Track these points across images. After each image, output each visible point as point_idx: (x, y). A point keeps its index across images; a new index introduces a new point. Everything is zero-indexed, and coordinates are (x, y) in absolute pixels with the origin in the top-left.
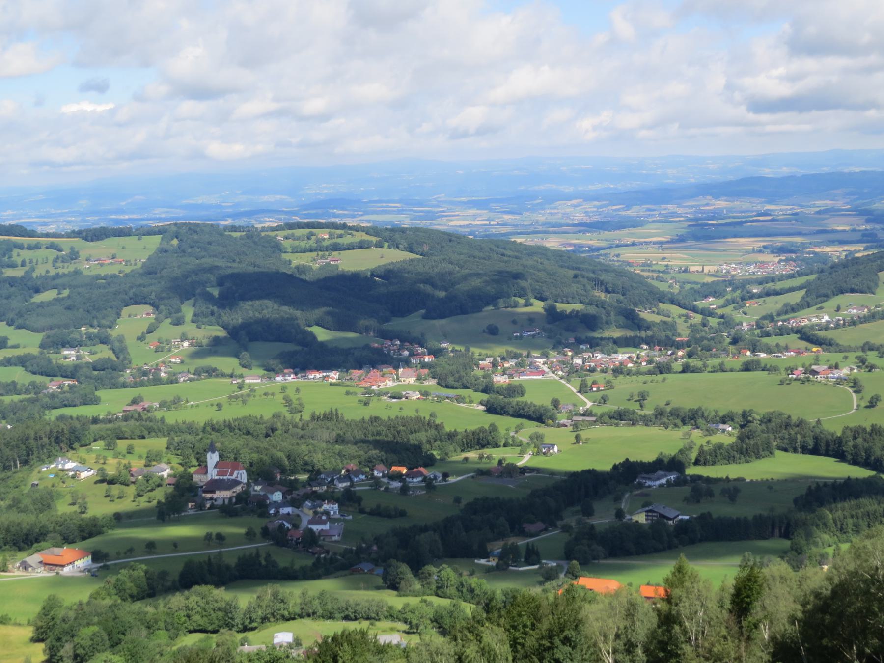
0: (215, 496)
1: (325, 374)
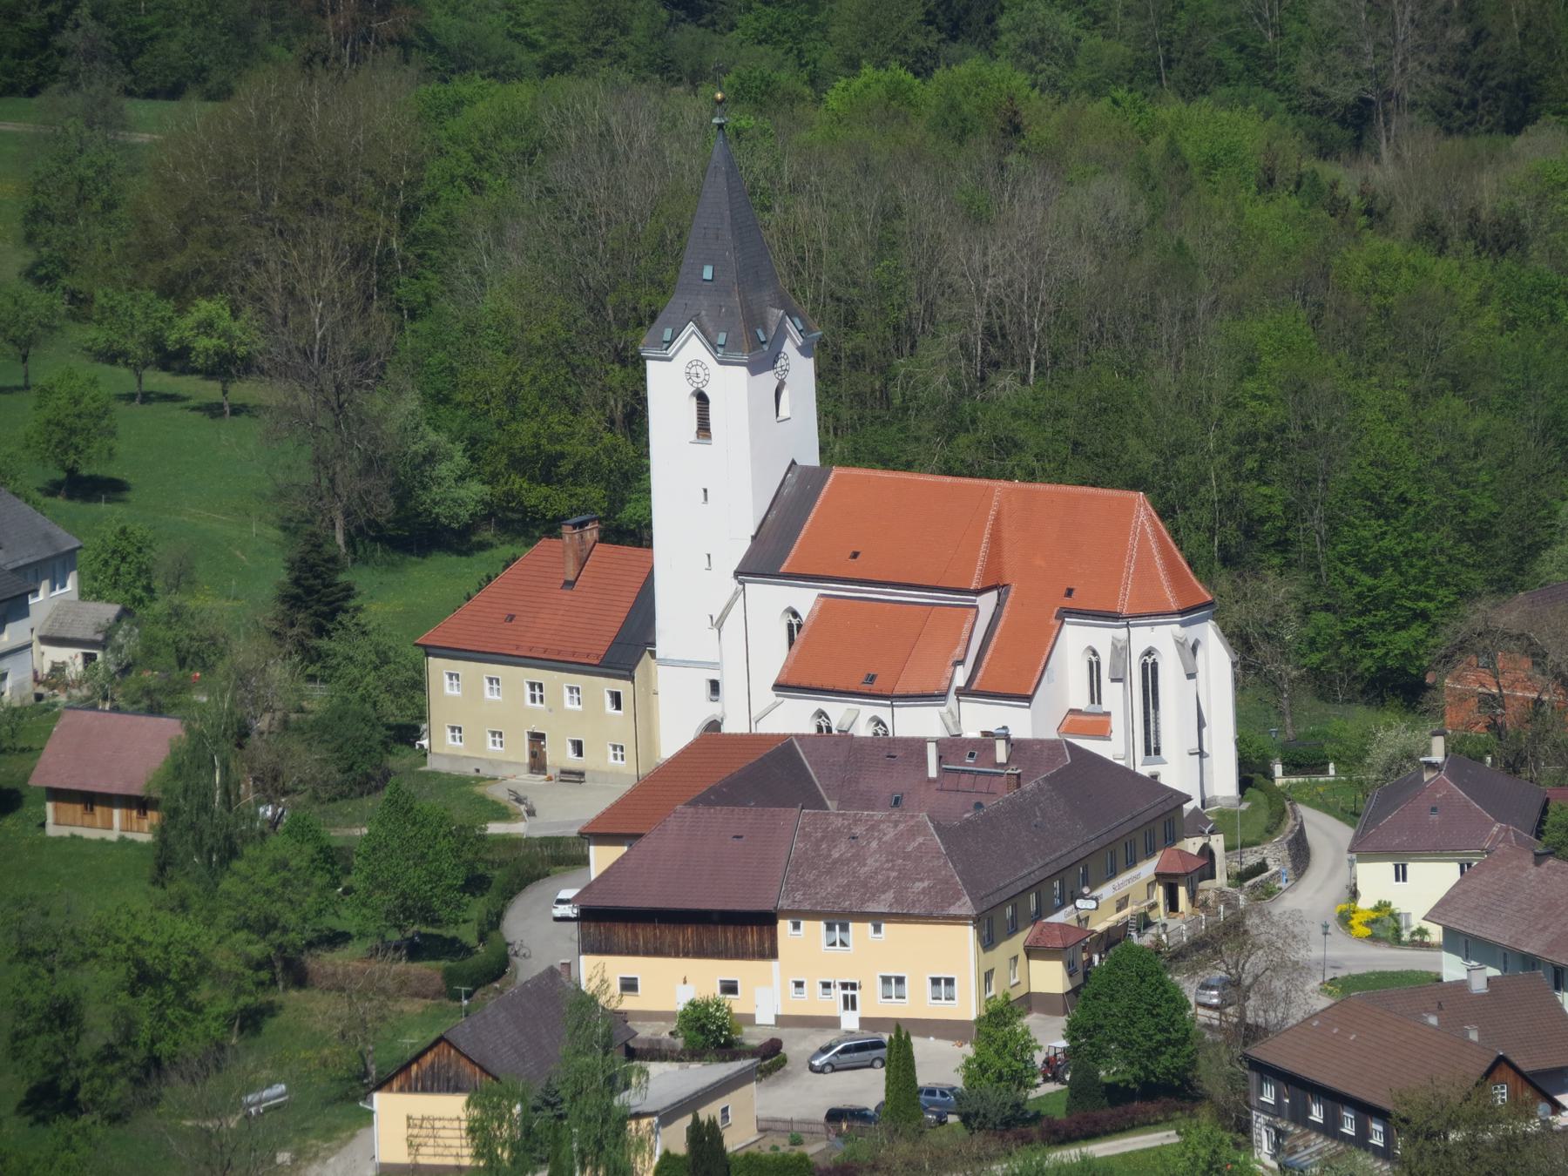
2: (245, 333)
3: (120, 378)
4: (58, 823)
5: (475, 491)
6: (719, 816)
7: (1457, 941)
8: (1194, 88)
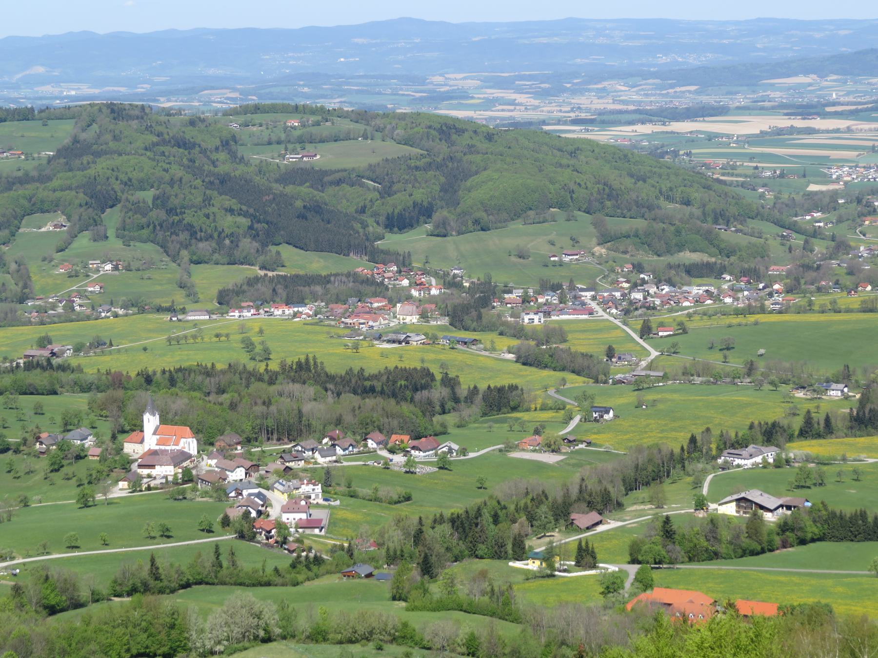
0: (153, 472)
1: (296, 309)
2: (108, 414)
3: (97, 418)
4: (90, 458)
5: (129, 428)
6: (151, 456)
7: (216, 467)
8: (194, 391)
